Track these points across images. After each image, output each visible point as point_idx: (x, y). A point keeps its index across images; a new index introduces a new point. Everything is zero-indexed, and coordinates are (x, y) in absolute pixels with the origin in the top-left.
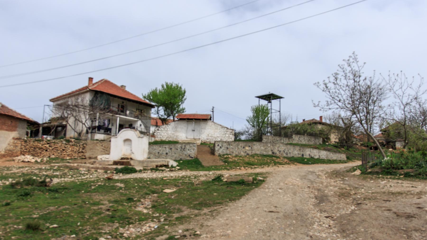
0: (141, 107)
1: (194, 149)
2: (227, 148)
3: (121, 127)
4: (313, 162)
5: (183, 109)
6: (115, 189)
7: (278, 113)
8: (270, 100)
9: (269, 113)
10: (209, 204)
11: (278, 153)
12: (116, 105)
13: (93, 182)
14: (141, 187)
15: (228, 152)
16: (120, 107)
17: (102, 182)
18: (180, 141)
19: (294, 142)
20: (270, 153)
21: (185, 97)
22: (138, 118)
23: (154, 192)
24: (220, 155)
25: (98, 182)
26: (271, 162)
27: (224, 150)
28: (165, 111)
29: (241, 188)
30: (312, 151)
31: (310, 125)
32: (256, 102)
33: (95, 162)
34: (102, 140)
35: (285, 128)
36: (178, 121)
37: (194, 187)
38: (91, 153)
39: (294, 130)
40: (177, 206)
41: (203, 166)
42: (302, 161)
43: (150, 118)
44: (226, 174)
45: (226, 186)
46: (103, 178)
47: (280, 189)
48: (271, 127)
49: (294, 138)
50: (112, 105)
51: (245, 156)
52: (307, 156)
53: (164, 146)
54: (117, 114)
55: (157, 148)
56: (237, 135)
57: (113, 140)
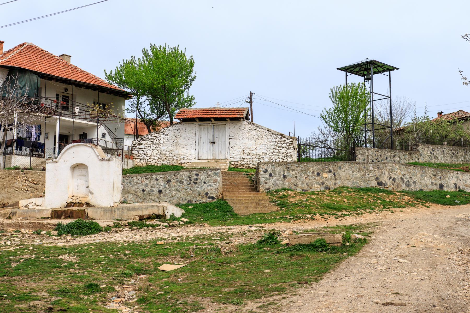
0: (104, 97)
1: (215, 181)
2: (284, 176)
3: (64, 140)
4: (463, 199)
5: (191, 99)
6: (59, 267)
7: (387, 101)
8: (369, 74)
9: (366, 102)
10: (257, 291)
11: (389, 183)
12: (52, 95)
13: (14, 253)
14: (111, 261)
15: (287, 185)
16: (60, 99)
17: (31, 253)
18: (187, 166)
19: (422, 160)
20: (374, 184)
21: (193, 74)
22: (98, 121)
23: (139, 271)
24: (269, 192)
25: (23, 253)
26: (376, 201)
27: (278, 180)
28: (151, 104)
29: (319, 258)
30: (460, 176)
31: (454, 123)
32: (340, 79)
33: (14, 213)
34: (26, 169)
35: (402, 131)
36: (180, 123)
37: (221, 259)
38: (5, 196)
39: (420, 134)
40: (191, 299)
41: (236, 215)
42: (440, 198)
43: (124, 120)
44: (284, 229)
45: (288, 254)
46: (32, 245)
47: (401, 256)
48: (373, 130)
49: (421, 151)
50: (43, 95)
51: (323, 192)
52: (450, 188)
53: (154, 177)
54: (54, 114)
55: (140, 181)
56: (302, 149)
57: (49, 166)
